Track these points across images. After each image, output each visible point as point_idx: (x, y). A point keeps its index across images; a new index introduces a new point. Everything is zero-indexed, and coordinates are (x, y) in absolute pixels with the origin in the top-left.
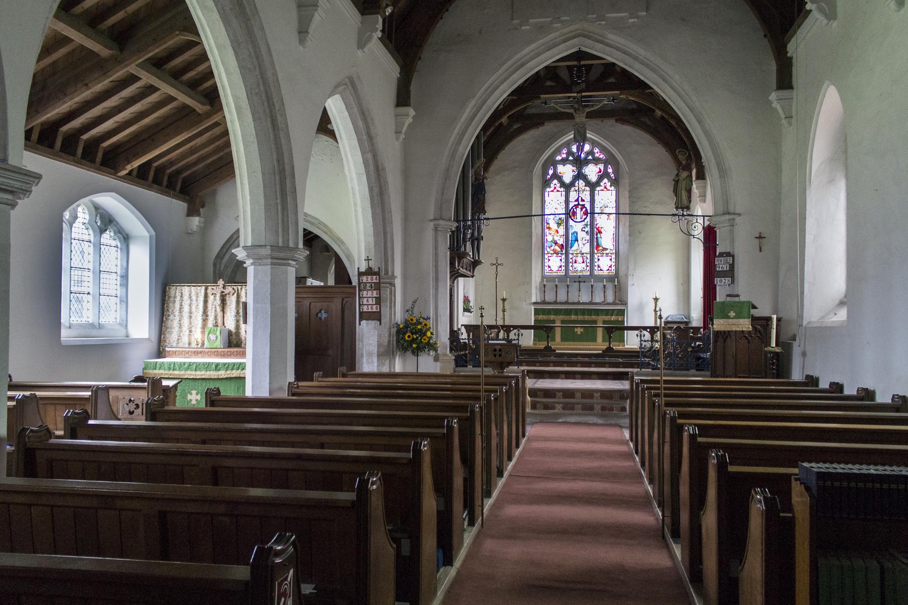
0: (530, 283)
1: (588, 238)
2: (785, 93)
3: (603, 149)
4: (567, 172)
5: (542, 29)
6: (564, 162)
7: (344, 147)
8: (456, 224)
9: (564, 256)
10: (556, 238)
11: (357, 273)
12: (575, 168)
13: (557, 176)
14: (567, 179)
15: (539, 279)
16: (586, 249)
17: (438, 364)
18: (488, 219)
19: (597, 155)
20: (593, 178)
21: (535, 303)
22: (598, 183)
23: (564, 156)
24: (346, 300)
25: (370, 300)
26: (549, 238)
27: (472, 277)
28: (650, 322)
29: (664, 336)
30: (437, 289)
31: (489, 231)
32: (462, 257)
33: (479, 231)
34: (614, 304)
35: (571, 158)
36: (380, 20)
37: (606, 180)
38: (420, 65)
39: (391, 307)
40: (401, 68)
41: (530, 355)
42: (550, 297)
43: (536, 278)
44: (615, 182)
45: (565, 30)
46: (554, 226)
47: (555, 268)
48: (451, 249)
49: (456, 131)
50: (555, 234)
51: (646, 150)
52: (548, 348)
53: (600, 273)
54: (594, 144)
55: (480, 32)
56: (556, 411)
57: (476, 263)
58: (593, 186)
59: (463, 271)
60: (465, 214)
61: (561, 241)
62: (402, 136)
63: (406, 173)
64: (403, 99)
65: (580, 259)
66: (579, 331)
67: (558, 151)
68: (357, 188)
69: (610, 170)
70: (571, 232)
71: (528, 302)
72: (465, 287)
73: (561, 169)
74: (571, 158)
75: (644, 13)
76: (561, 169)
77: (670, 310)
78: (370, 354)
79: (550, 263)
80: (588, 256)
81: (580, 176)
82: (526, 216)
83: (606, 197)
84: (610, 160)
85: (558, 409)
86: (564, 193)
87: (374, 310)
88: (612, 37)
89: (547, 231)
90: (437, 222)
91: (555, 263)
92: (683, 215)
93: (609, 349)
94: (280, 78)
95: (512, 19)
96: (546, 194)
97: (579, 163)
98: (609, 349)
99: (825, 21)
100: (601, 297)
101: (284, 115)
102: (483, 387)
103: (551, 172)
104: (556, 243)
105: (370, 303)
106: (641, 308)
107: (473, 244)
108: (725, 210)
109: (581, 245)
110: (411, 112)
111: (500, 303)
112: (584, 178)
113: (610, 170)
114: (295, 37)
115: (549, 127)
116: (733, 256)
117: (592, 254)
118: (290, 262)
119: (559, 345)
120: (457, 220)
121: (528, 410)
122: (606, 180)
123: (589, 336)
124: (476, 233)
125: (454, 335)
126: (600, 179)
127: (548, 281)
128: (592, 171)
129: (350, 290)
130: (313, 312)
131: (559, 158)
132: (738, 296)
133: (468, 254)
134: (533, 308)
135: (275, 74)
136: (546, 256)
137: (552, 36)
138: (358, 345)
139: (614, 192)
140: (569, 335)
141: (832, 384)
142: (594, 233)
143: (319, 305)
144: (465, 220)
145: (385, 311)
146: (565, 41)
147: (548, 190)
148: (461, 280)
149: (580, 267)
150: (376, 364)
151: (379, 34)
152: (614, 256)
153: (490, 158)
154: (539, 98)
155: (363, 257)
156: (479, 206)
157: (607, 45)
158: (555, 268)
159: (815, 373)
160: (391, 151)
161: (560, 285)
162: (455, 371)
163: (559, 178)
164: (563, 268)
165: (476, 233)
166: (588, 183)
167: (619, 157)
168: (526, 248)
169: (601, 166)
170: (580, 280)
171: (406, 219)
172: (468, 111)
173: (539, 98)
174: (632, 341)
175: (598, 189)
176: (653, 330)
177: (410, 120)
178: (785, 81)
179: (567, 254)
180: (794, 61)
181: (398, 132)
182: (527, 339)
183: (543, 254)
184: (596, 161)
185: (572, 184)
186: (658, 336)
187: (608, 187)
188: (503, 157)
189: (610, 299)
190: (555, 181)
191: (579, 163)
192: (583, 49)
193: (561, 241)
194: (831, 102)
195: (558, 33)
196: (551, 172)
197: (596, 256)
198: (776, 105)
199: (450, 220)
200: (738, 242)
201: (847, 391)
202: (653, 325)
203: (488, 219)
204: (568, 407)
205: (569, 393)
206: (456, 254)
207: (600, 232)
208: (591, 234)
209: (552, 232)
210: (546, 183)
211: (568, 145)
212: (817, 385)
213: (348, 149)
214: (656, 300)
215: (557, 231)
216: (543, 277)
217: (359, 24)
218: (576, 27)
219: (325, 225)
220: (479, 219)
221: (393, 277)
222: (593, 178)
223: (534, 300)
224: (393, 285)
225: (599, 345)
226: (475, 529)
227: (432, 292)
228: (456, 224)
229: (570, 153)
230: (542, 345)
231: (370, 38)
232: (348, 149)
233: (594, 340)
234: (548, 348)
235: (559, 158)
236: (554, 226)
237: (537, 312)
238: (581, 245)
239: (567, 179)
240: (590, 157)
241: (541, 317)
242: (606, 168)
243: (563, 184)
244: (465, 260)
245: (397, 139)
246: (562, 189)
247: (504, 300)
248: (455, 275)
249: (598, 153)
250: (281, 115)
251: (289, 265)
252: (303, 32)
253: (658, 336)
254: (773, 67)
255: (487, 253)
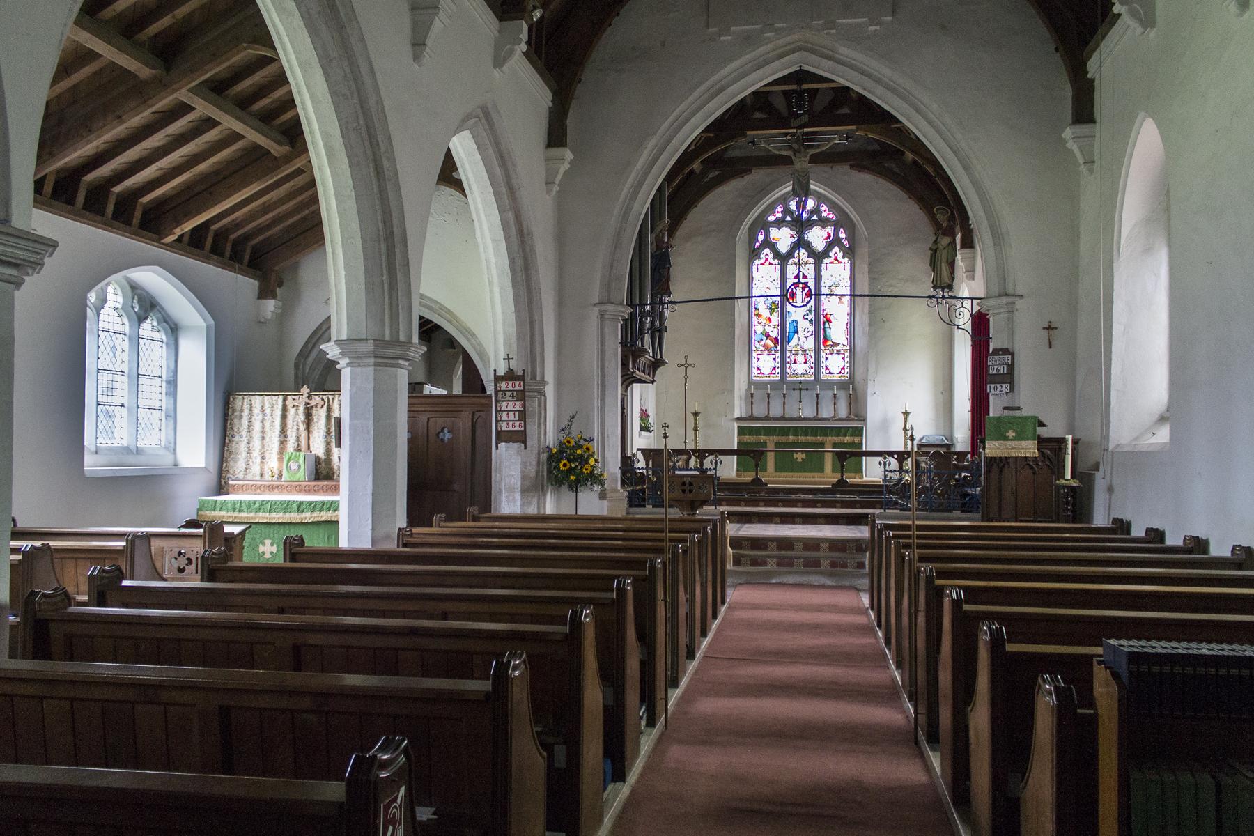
0: (732, 391)
1: (812, 328)
2: (1084, 129)
3: (833, 206)
4: (783, 237)
5: (749, 41)
6: (779, 223)
7: (475, 204)
8: (630, 310)
9: (778, 354)
10: (768, 329)
11: (492, 377)
12: (793, 233)
13: (769, 244)
14: (784, 247)
15: (744, 386)
16: (810, 344)
17: (605, 503)
18: (674, 303)
19: (824, 214)
20: (819, 245)
21: (738, 419)
22: (825, 253)
23: (779, 215)
24: (478, 414)
25: (511, 414)
26: (759, 329)
27: (653, 382)
28: (898, 445)
29: (917, 464)
30: (603, 399)
31: (675, 319)
32: (638, 355)
33: (662, 320)
34: (848, 419)
35: (788, 218)
36: (525, 28)
37: (836, 249)
38: (579, 89)
39: (539, 424)
40: (555, 94)
41: (732, 491)
42: (759, 411)
43: (740, 384)
44: (850, 252)
45: (780, 42)
46: (765, 312)
47: (766, 371)
48: (623, 344)
49: (630, 181)
50: (766, 324)
51: (891, 206)
52: (757, 481)
53: (829, 377)
54: (820, 199)
55: (663, 44)
56: (768, 568)
57: (657, 364)
58: (819, 257)
59: (639, 374)
60: (642, 296)
61: (775, 333)
62: (556, 188)
63: (561, 239)
64: (556, 136)
65: (800, 358)
66: (800, 457)
67: (771, 209)
68: (493, 260)
69: (842, 236)
70: (788, 320)
71: (730, 417)
72: (642, 396)
73: (774, 233)
74: (788, 218)
75: (890, 18)
76: (774, 233)
77: (925, 428)
78: (511, 490)
79: (760, 364)
80: (813, 354)
81: (801, 243)
82: (726, 298)
83: (837, 273)
84: (843, 221)
85: (771, 566)
86: (778, 267)
87: (517, 428)
88: (845, 51)
89: (755, 319)
90: (603, 307)
91: (766, 364)
92: (943, 297)
93: (841, 482)
94: (386, 108)
95: (707, 27)
96: (755, 268)
97: (800, 225)
98: (841, 482)
99: (1139, 30)
100: (831, 410)
101: (392, 159)
102: (667, 535)
103: (761, 238)
104: (768, 336)
105: (512, 418)
106: (885, 425)
107: (653, 338)
108: (1002, 290)
109: (803, 339)
110: (568, 154)
111: (691, 418)
112: (807, 246)
113: (842, 236)
114: (407, 51)
115: (758, 176)
116: (1012, 354)
117: (817, 351)
118: (401, 362)
119: (773, 477)
120: (631, 304)
121: (730, 566)
122: (836, 249)
123: (814, 464)
124: (658, 322)
125: (627, 463)
126: (829, 247)
127: (756, 389)
128: (817, 237)
129: (483, 401)
130: (433, 431)
131: (772, 218)
132: (1019, 409)
133: (646, 351)
134: (736, 425)
135: (380, 102)
136: (754, 354)
137: (762, 49)
138: (495, 476)
139: (848, 266)
140: (785, 462)
141: (1149, 531)
142: (821, 321)
143: (440, 421)
144: (642, 304)
145: (532, 430)
146: (780, 57)
147: (757, 262)
148: (637, 386)
149: (801, 369)
150: (519, 503)
151: (524, 47)
152: (847, 354)
153: (677, 219)
154: (745, 135)
155: (502, 355)
156: (662, 285)
157: (839, 62)
158: (766, 371)
159: (1126, 516)
160: (540, 209)
161: (773, 394)
162: (628, 513)
163: (772, 246)
164: (778, 371)
165: (658, 322)
166: (812, 253)
167: (855, 216)
168: (726, 342)
169: (831, 230)
170: (801, 387)
171: (561, 303)
172: (646, 152)
173: (745, 135)
174: (873, 472)
175: (826, 261)
176: (901, 456)
177: (566, 166)
178: (1084, 112)
179: (783, 351)
180: (1096, 84)
181: (549, 183)
182: (728, 469)
183: (750, 351)
184: (823, 222)
185: (790, 254)
186: (909, 464)
187: (840, 259)
188: (695, 217)
189: (843, 413)
190: (767, 251)
191: (800, 225)
192: (805, 67)
193: (775, 333)
194: (1147, 142)
195: (770, 46)
196: (761, 238)
197: (823, 354)
198: (1072, 145)
199: (621, 304)
200: (1020, 334)
201: (1170, 541)
202: (902, 449)
203: (674, 303)
204: (785, 563)
205: (785, 544)
206: (630, 351)
207: (829, 321)
208: (817, 323)
209: (763, 320)
210: (754, 253)
211: (784, 200)
212: (1128, 532)
213: (480, 206)
214: (906, 414)
215: (769, 320)
216: (750, 383)
217: (496, 33)
218: (796, 37)
219: (449, 311)
220: (662, 303)
221: (543, 383)
222: (819, 245)
223: (737, 415)
224: (542, 393)
225: (827, 477)
226: (656, 732)
227: (596, 403)
228: (630, 310)
229: (787, 211)
230: (748, 477)
231: (511, 52)
232: (480, 206)
233: (821, 469)
234: (757, 481)
235: (772, 218)
236: (765, 312)
237: (742, 431)
238: (803, 339)
239: (784, 247)
240: (815, 217)
241: (747, 438)
242: (836, 232)
243: (777, 255)
244: (642, 359)
245: (548, 192)
246: (777, 261)
247: (696, 414)
248: (628, 380)
249: (825, 212)
250: (388, 159)
251: (399, 366)
252: (418, 44)
253: (909, 464)
254: (1068, 92)
255: (672, 350)
